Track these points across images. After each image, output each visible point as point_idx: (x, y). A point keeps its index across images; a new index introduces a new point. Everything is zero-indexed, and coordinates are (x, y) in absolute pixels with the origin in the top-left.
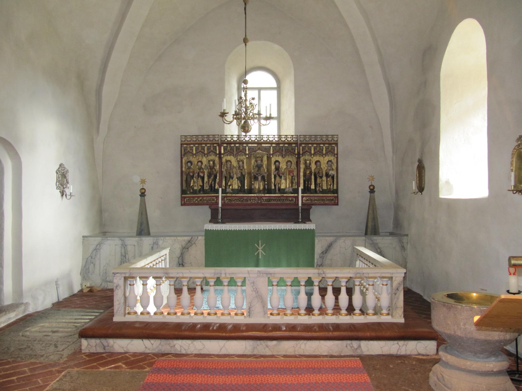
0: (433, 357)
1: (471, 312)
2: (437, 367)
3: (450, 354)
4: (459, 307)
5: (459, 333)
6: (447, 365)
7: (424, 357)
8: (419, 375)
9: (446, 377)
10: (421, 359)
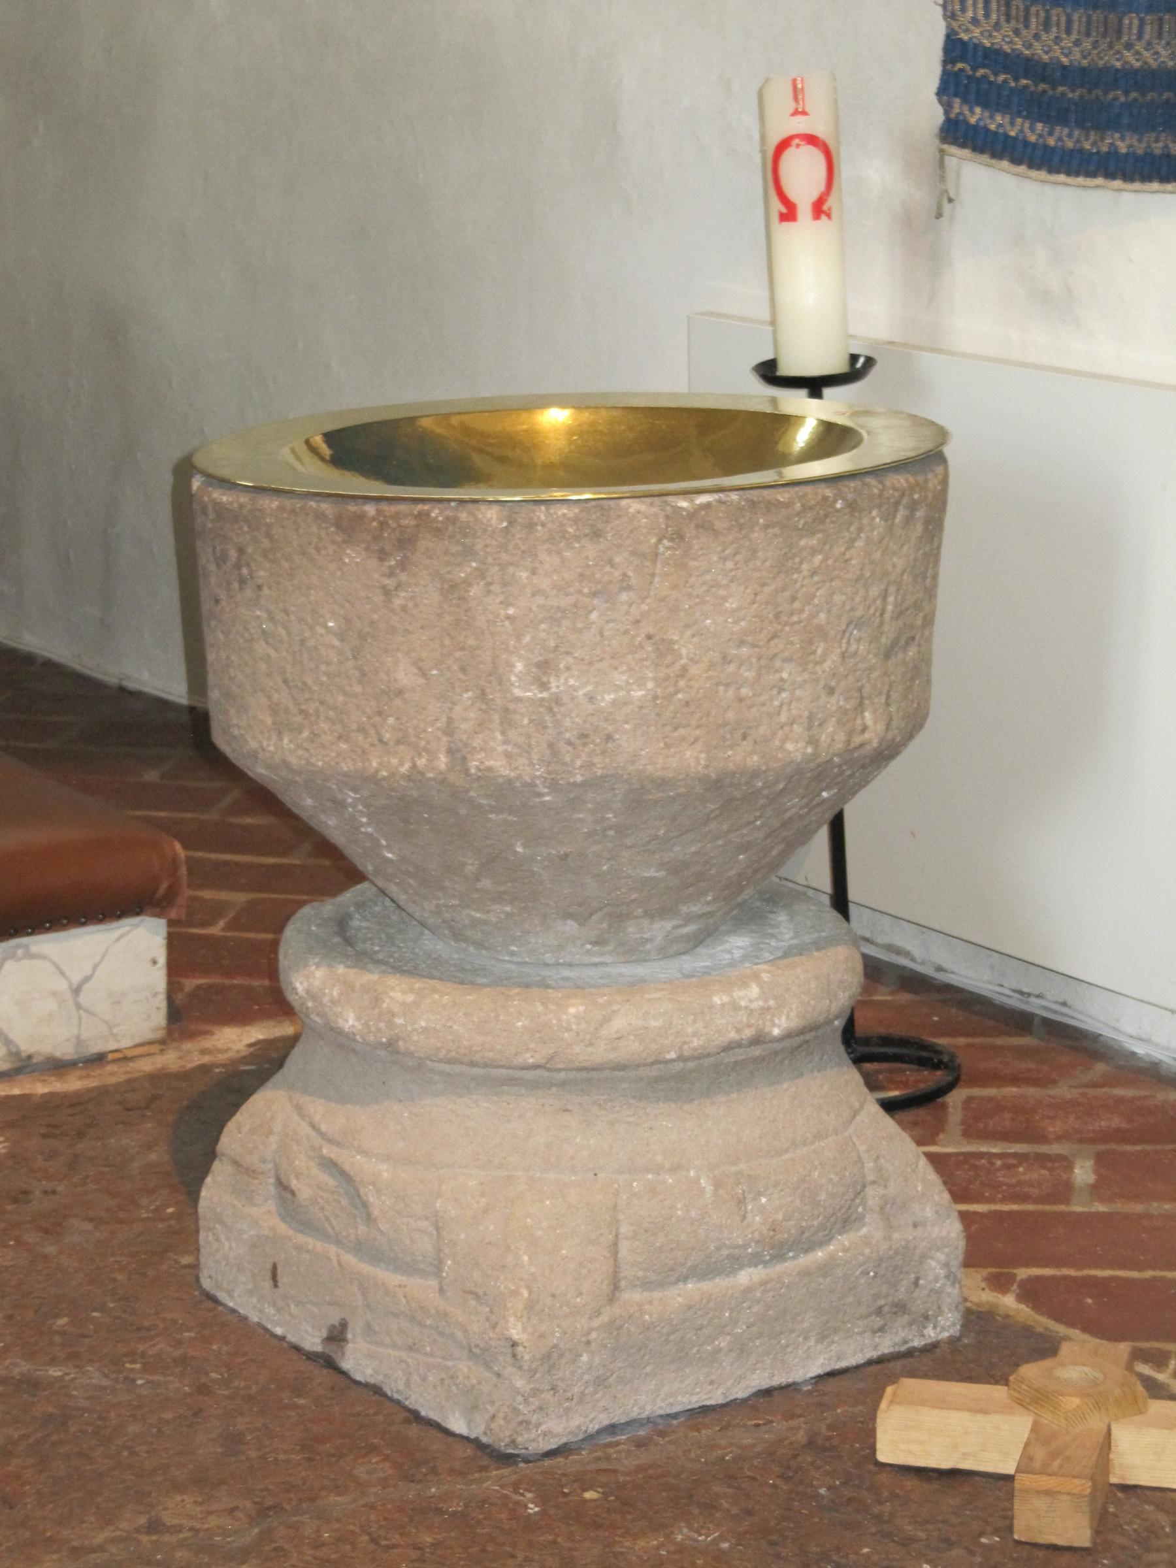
0: (147, 1066)
1: (591, 550)
2: (267, 1125)
3: (397, 970)
4: (491, 515)
5: (495, 757)
6: (388, 1066)
7: (73, 1084)
8: (79, 1231)
9: (385, 1172)
10: (51, 1103)
